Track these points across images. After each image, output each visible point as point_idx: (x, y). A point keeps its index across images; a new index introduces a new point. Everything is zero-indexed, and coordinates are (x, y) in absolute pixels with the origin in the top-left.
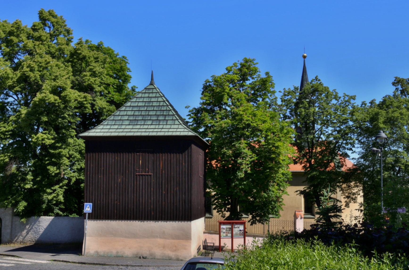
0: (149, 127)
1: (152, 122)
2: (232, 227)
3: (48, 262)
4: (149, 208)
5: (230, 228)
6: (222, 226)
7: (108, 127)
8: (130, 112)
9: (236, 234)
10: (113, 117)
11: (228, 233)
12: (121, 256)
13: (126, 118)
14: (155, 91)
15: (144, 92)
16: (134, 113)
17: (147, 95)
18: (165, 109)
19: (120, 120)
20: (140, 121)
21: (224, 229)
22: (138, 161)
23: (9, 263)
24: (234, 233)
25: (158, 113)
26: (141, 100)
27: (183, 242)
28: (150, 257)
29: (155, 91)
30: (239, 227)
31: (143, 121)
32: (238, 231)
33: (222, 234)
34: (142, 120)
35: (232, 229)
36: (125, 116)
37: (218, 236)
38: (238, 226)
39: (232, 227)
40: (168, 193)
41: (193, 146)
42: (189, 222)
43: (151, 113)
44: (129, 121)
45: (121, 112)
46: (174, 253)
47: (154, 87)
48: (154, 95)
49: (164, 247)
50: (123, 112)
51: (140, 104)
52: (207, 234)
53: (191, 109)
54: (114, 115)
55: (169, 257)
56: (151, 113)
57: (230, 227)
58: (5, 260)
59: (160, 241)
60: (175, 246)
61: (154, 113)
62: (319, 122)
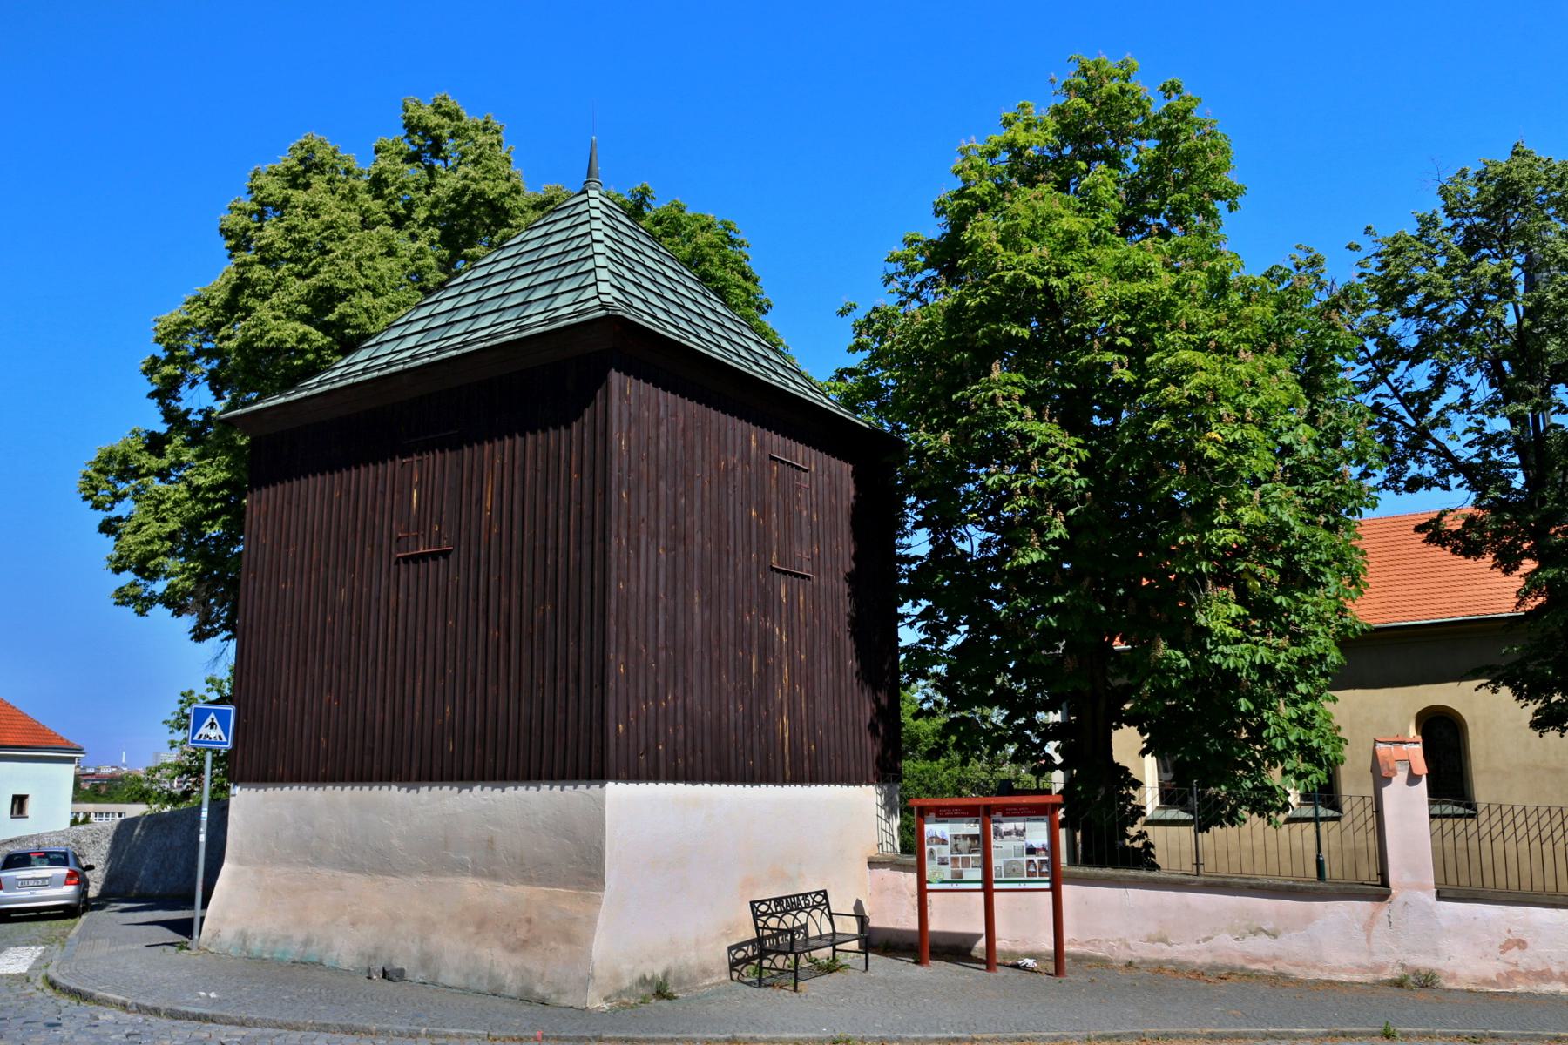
2: (985, 830)
4: (438, 721)
5: (973, 837)
6: (932, 829)
9: (1010, 869)
11: (966, 863)
12: (315, 959)
21: (944, 842)
22: (407, 491)
24: (997, 862)
27: (563, 900)
28: (420, 976)
30: (1020, 833)
32: (1017, 853)
33: (931, 868)
35: (982, 843)
37: (911, 878)
38: (1020, 825)
39: (985, 830)
40: (509, 640)
41: (615, 377)
42: (595, 788)
46: (517, 960)
49: (481, 924)
52: (886, 873)
53: (860, 315)
55: (492, 978)
57: (975, 829)
59: (472, 889)
60: (529, 921)
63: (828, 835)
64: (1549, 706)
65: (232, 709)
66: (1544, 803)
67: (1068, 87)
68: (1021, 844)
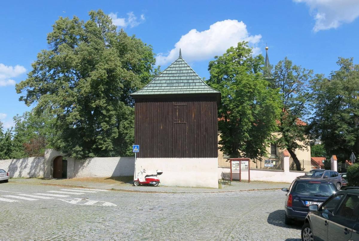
0: (183, 88)
1: (184, 84)
3: (107, 191)
5: (238, 164)
7: (152, 88)
8: (167, 77)
10: (154, 81)
13: (164, 82)
14: (183, 62)
15: (175, 63)
16: (170, 78)
17: (178, 66)
18: (193, 75)
19: (154, 83)
20: (175, 84)
21: (234, 164)
23: (79, 192)
24: (241, 167)
25: (188, 78)
26: (174, 69)
29: (183, 62)
30: (245, 163)
31: (177, 84)
34: (177, 83)
36: (163, 81)
43: (182, 78)
44: (167, 84)
45: (160, 78)
47: (182, 60)
48: (183, 65)
50: (162, 77)
51: (173, 72)
54: (154, 80)
56: (182, 78)
58: (74, 189)
61: (185, 78)
62: (25, 124)
63: (53, 170)
64: (96, 144)
65: (139, 145)
66: (307, 160)
67: (142, 77)
68: (245, 165)
